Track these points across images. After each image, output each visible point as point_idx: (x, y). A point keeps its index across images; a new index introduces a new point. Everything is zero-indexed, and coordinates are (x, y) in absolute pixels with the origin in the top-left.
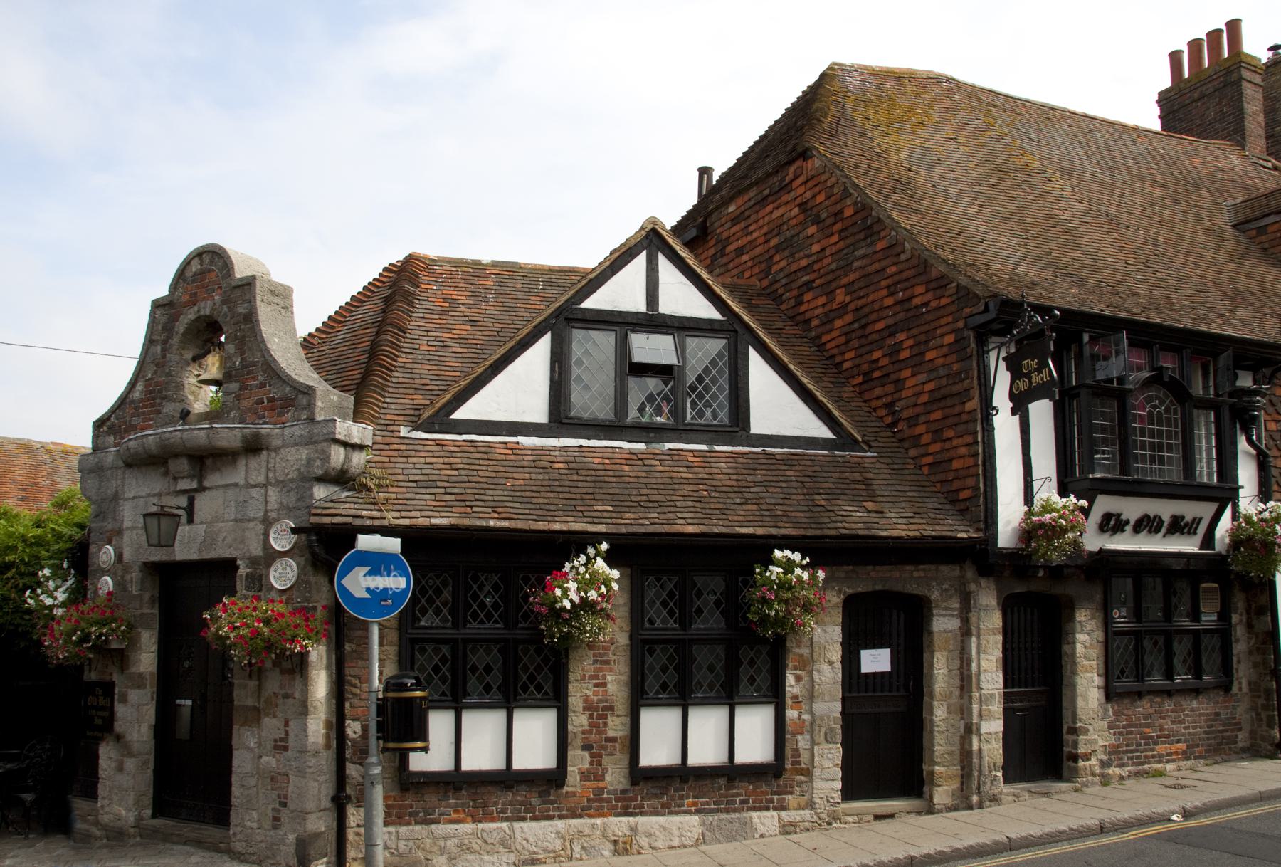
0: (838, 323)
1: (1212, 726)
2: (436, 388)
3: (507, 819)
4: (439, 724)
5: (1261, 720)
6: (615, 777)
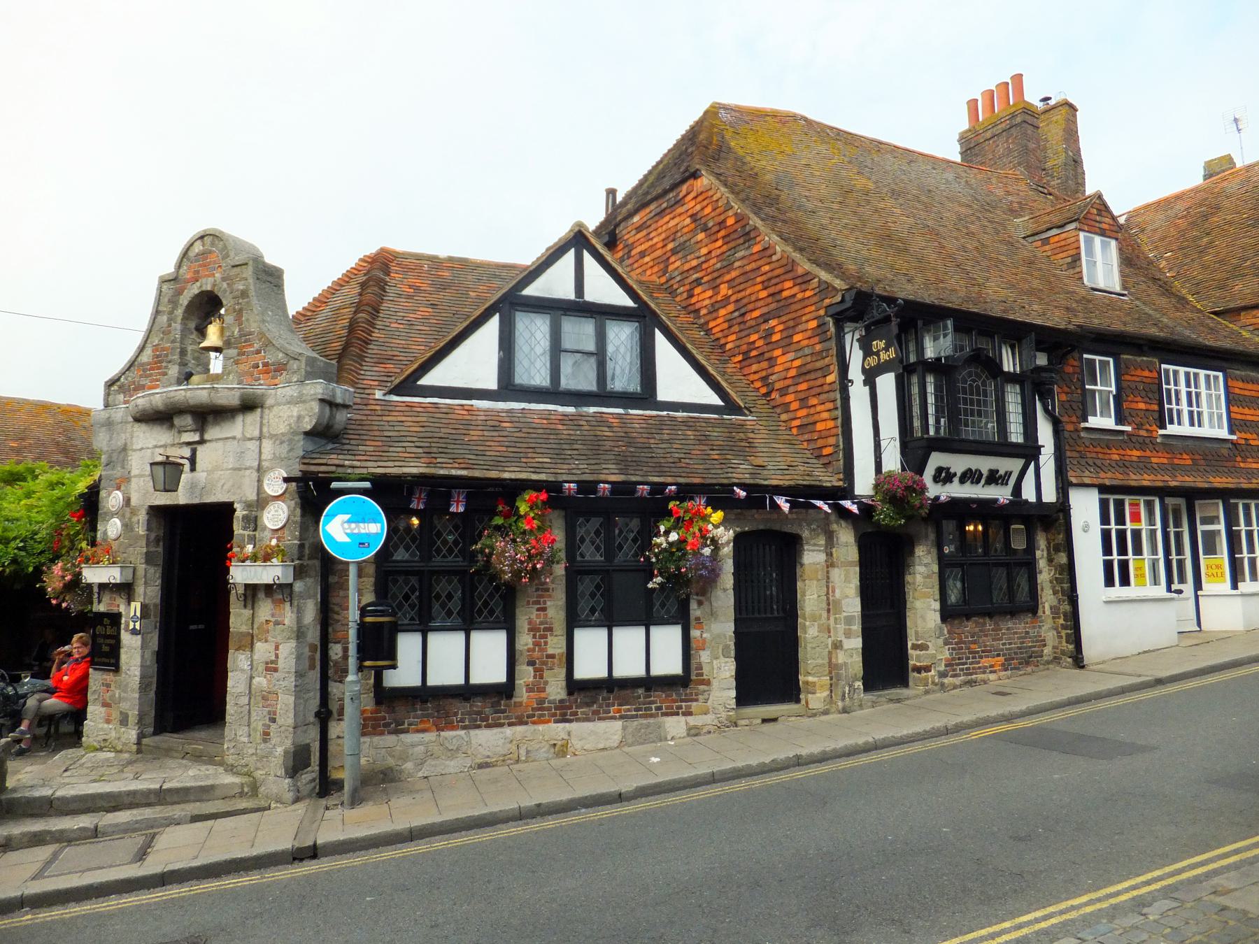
0: (722, 312)
1: (1023, 643)
2: (405, 359)
3: (464, 728)
4: (408, 645)
5: (1061, 637)
6: (556, 689)
